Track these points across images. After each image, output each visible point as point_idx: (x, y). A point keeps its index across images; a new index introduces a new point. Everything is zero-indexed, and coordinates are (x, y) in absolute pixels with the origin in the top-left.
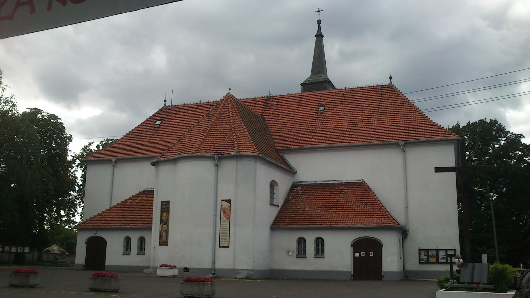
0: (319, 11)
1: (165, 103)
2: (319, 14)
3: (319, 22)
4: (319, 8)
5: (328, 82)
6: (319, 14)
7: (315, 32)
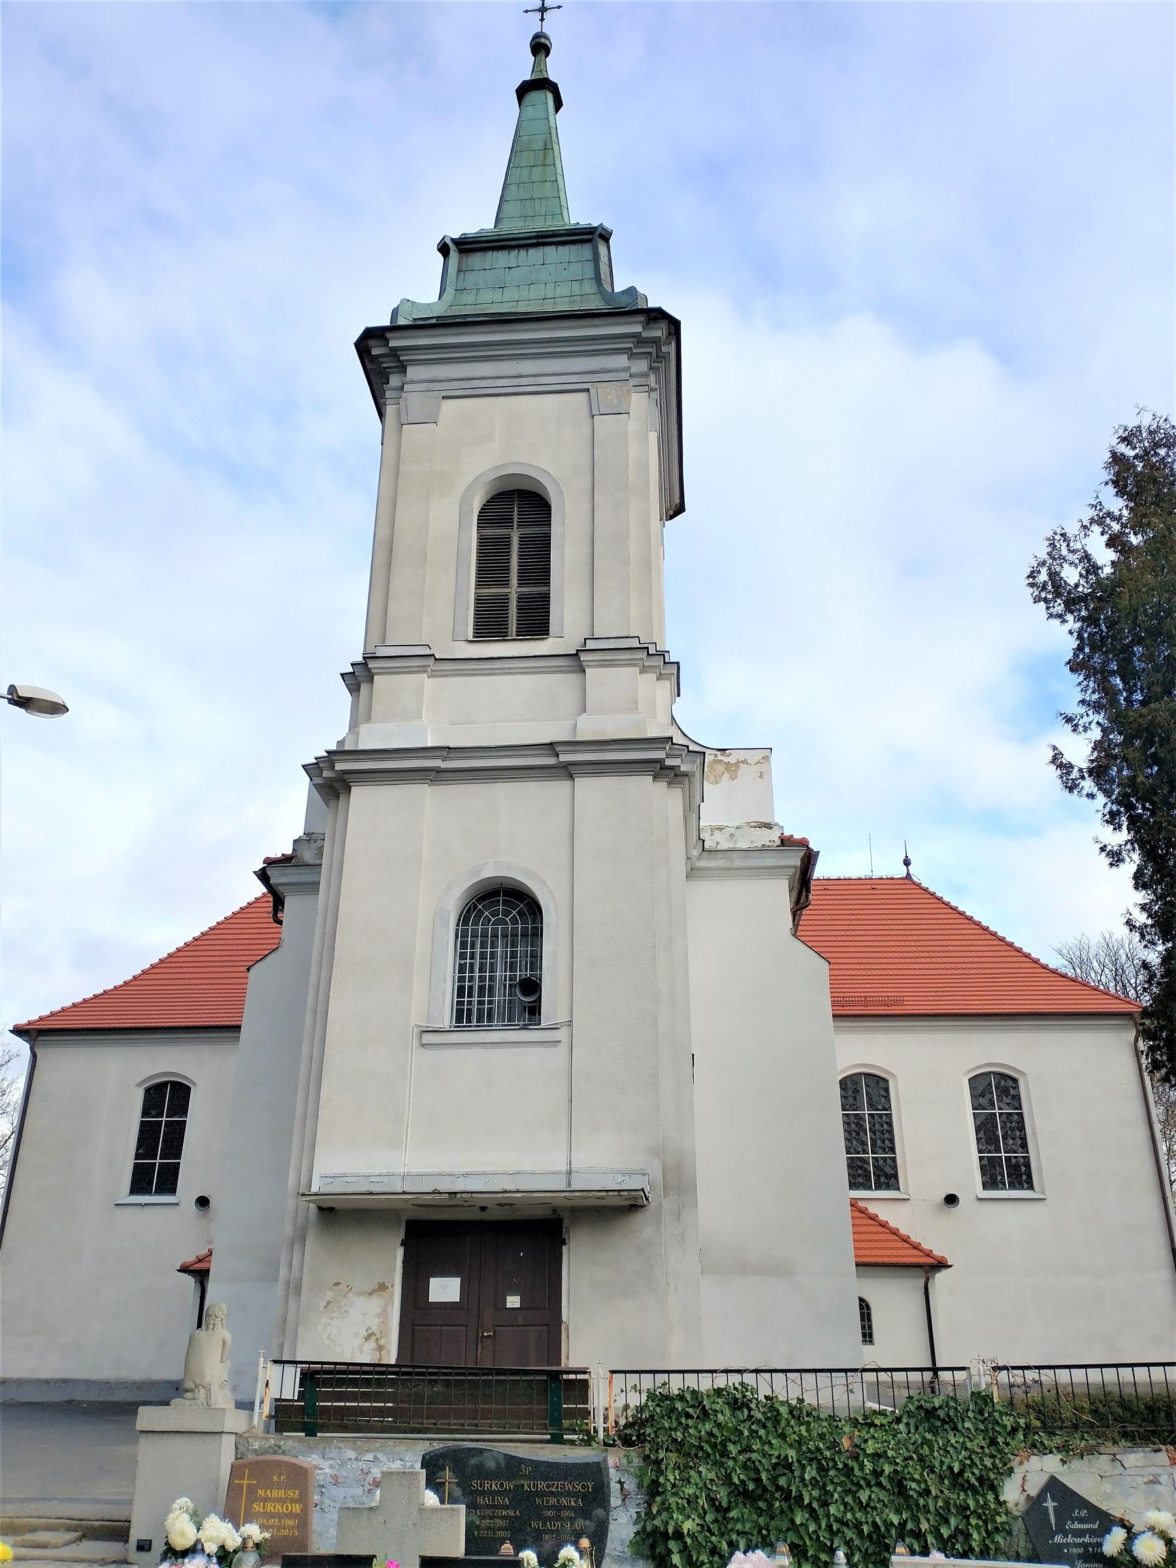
2: (542, 20)
6: (542, 20)
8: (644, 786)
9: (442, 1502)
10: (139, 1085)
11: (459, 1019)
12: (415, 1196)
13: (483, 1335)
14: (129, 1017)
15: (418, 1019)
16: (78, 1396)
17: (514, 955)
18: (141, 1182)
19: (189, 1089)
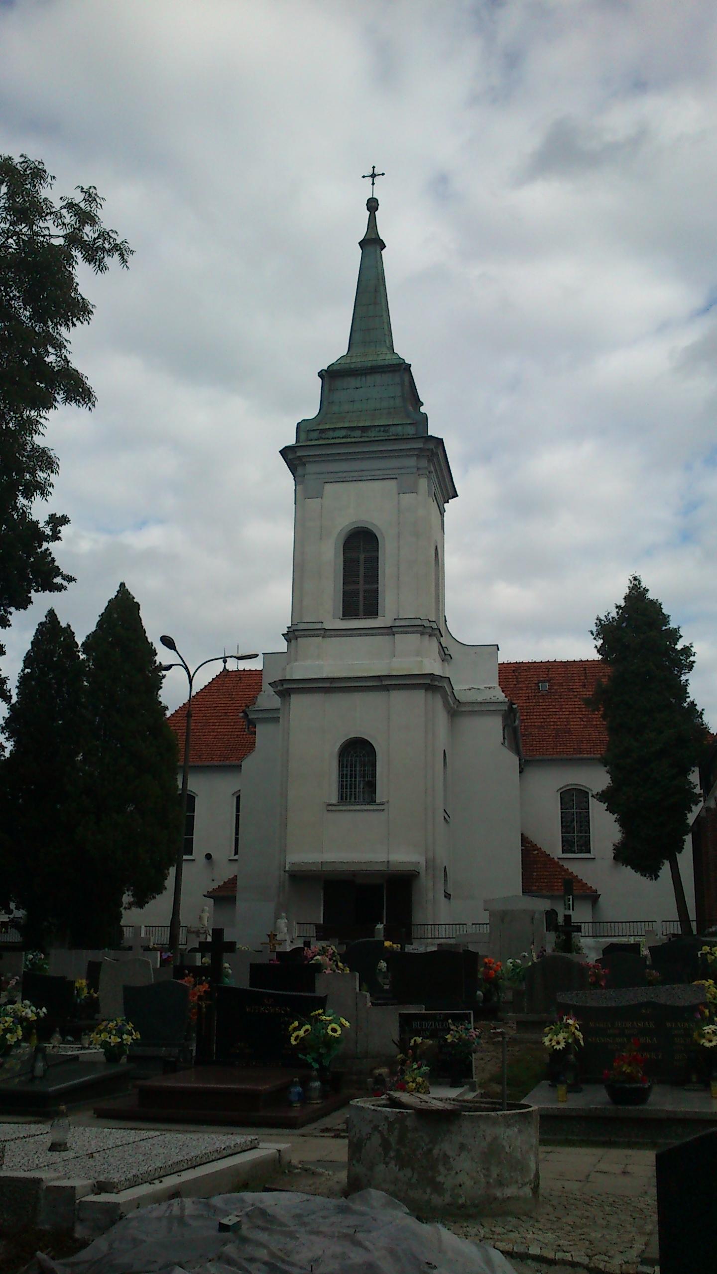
0: (373, 176)
1: (225, 666)
2: (373, 184)
3: (372, 205)
4: (374, 167)
5: (198, 1004)
6: (373, 184)
7: (361, 232)
8: (419, 696)
9: (499, 664)
11: (342, 799)
17: (364, 771)
19: (194, 798)
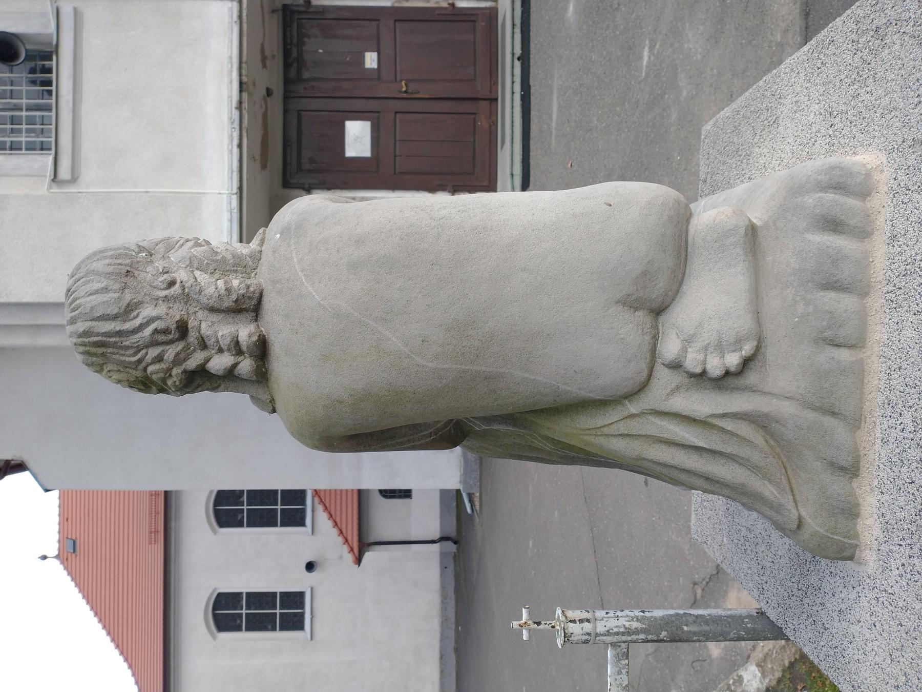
10: (214, 637)
11: (43, 147)
12: (245, 134)
13: (406, 92)
14: (90, 578)
15: (43, 188)
16: (451, 644)
18: (294, 623)
19: (220, 595)
